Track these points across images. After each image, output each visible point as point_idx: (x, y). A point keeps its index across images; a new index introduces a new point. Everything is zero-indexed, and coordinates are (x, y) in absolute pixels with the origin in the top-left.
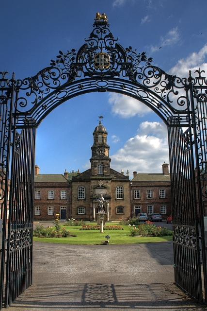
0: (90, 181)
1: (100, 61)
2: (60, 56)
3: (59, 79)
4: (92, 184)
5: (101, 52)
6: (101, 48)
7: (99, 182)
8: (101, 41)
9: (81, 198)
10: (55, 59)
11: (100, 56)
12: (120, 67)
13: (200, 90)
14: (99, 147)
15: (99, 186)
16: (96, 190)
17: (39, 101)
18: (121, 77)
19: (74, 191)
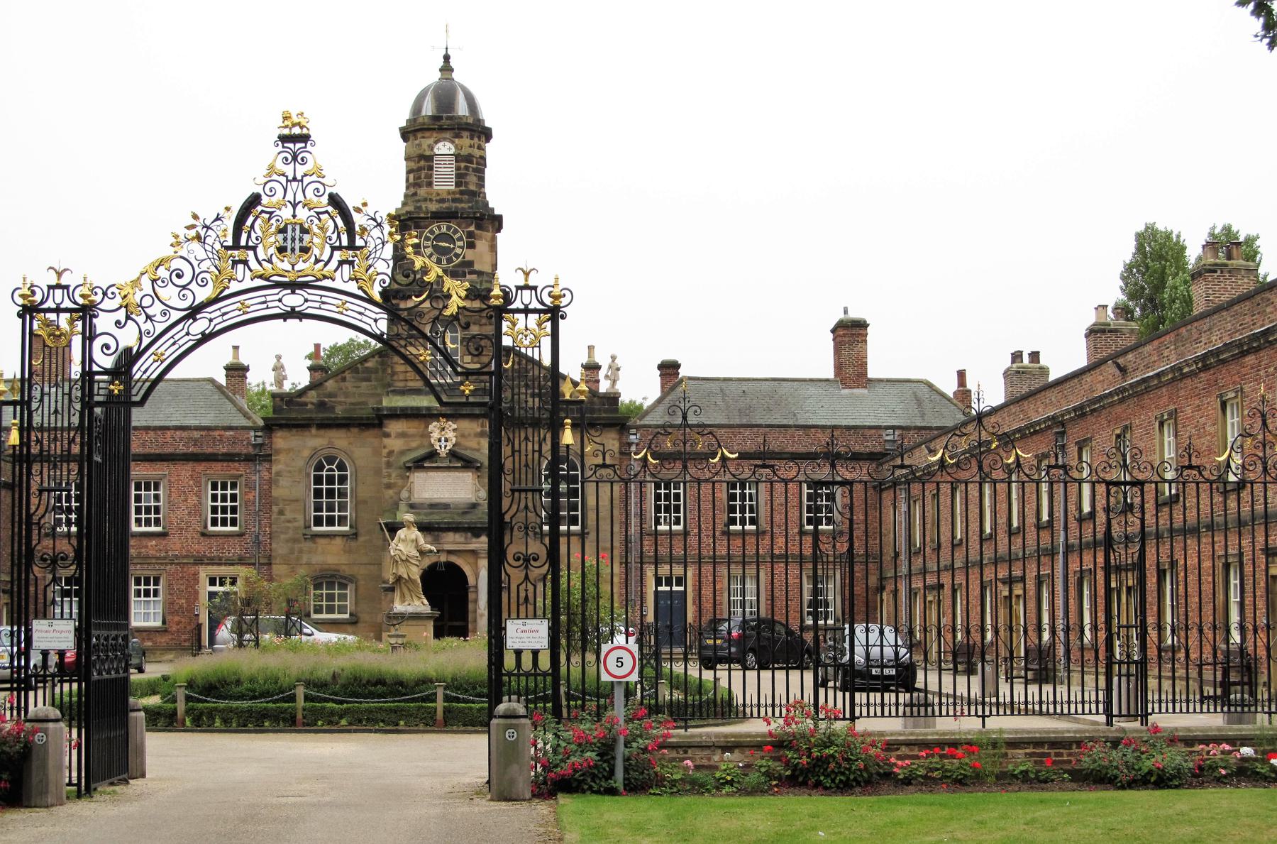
0: (380, 425)
1: (289, 241)
2: (193, 227)
3: (193, 286)
4: (395, 444)
5: (294, 216)
6: (294, 206)
7: (434, 427)
8: (295, 184)
9: (331, 521)
10: (182, 232)
11: (290, 228)
12: (337, 254)
13: (521, 316)
14: (438, 216)
15: (433, 455)
16: (418, 478)
17: (146, 341)
18: (338, 284)
19: (283, 482)
